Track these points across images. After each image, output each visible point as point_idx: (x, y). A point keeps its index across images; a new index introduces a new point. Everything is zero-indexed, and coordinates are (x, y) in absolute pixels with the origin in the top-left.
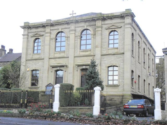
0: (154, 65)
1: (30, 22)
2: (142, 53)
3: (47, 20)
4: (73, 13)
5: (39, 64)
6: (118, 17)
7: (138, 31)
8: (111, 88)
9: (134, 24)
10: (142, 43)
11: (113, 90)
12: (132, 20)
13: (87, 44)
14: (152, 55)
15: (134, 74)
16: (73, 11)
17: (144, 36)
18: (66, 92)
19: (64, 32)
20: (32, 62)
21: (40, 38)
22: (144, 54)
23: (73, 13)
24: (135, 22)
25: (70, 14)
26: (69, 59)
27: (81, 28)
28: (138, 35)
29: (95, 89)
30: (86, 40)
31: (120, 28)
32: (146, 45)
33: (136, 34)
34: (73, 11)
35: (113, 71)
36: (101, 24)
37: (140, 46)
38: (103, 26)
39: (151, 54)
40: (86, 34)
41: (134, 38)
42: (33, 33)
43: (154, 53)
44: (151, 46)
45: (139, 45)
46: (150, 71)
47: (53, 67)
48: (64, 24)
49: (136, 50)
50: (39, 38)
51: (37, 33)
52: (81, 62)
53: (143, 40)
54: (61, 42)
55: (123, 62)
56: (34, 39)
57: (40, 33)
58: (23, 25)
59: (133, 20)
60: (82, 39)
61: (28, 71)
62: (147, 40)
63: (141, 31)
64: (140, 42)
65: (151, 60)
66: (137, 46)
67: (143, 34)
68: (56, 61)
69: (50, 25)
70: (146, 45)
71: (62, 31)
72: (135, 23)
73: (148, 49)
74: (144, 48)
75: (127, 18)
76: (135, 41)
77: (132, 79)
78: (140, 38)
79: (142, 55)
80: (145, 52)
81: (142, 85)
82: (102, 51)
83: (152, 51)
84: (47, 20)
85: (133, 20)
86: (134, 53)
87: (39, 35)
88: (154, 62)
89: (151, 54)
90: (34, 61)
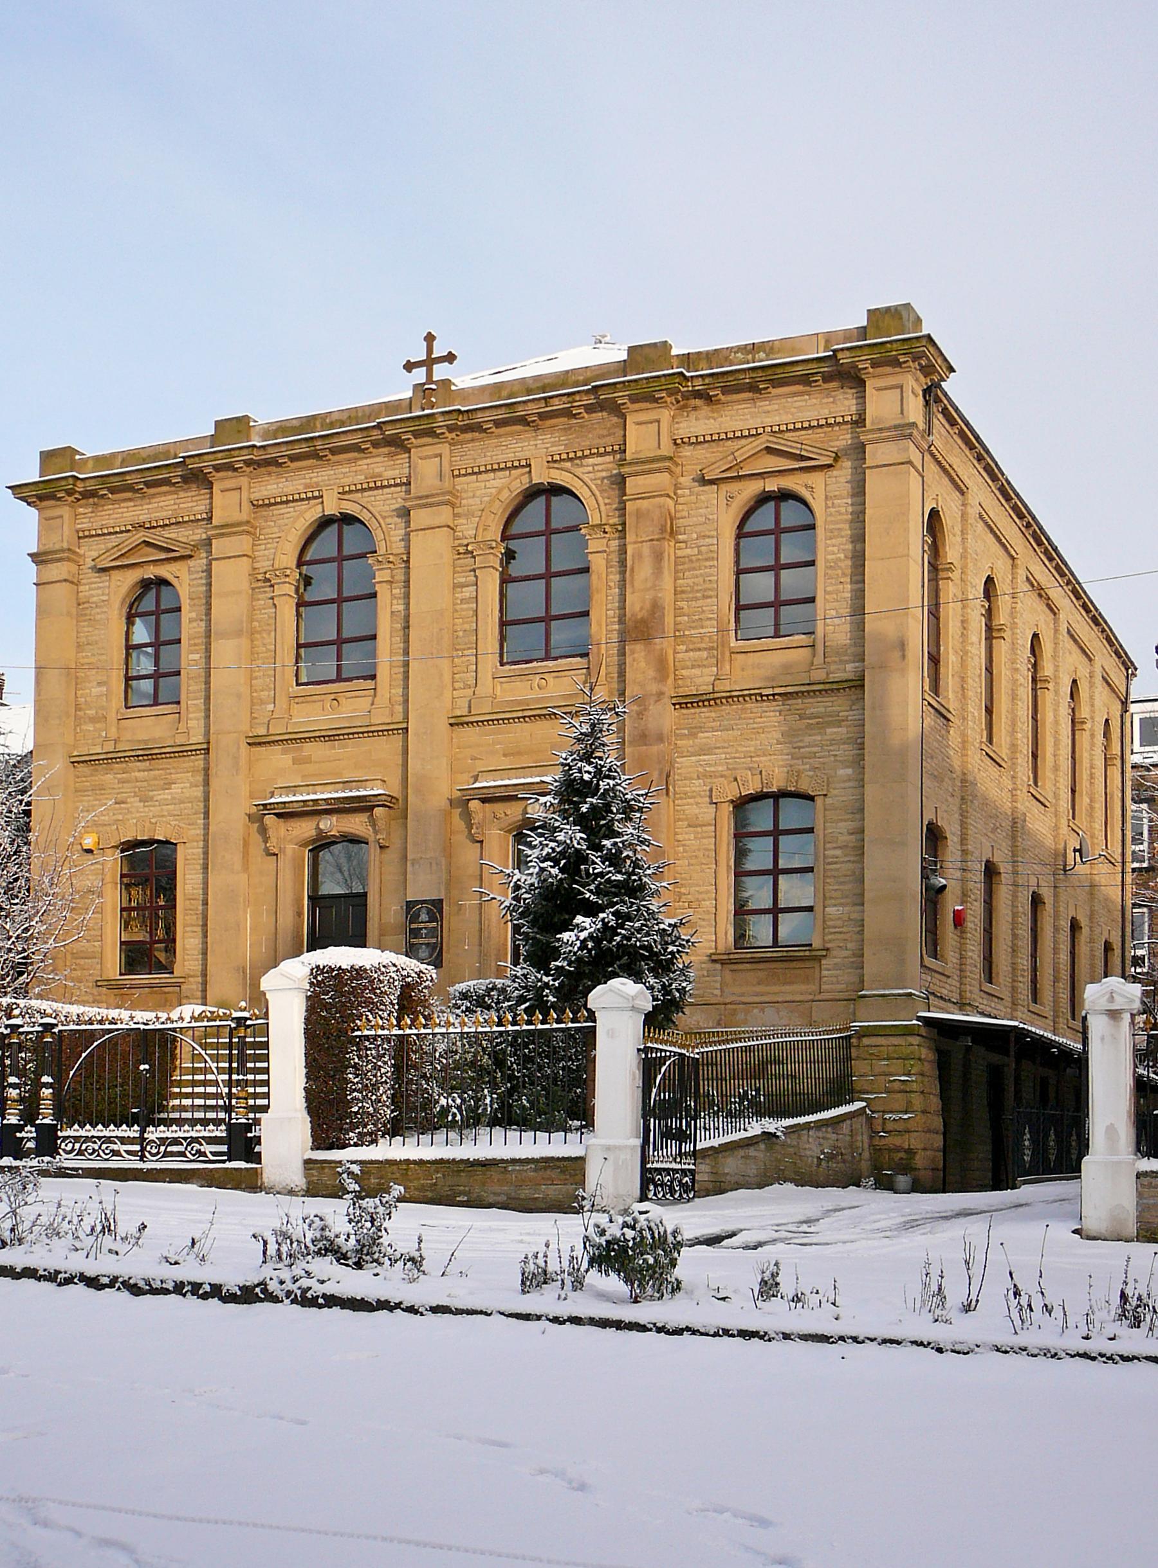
0: (1115, 772)
1: (90, 448)
2: (1015, 681)
3: (218, 424)
4: (430, 350)
5: (176, 789)
6: (805, 380)
7: (981, 492)
8: (761, 974)
9: (942, 437)
10: (1014, 596)
11: (776, 989)
12: (927, 403)
13: (554, 612)
14: (1101, 694)
15: (952, 851)
16: (430, 338)
17: (1038, 537)
18: (13, 1080)
19: (364, 516)
20: (121, 781)
21: (170, 578)
22: (1034, 680)
23: (430, 350)
24: (953, 416)
25: (409, 366)
26: (245, 727)
27: (496, 481)
28: (1067, 638)
29: (598, 997)
30: (548, 576)
31: (830, 466)
32: (1052, 609)
33: (964, 516)
34: (430, 338)
35: (770, 840)
36: (666, 441)
37: (1002, 618)
38: (687, 451)
39: (1092, 685)
40: (548, 532)
41: (951, 553)
42: (114, 540)
43: (1118, 679)
44: (1097, 620)
45: (989, 614)
46: (1082, 821)
47: (286, 814)
48: (356, 448)
49: (964, 655)
50: (162, 582)
51: (150, 537)
52: (506, 763)
53: (1022, 574)
54: (340, 600)
55: (859, 761)
56: (124, 589)
57: (172, 533)
58: (31, 474)
59: (933, 394)
60: (515, 569)
61: (89, 851)
62: (1061, 569)
63: (1006, 492)
64: (1083, 686)
65: (1092, 736)
66: (977, 623)
67: (1021, 512)
68: (308, 760)
69: (248, 463)
70: (1052, 609)
71: (350, 508)
72: (952, 423)
73: (1070, 644)
74: (989, 581)
75: (881, 383)
76: (956, 575)
77: (933, 896)
78: (1001, 552)
79: (1014, 697)
80: (1047, 669)
81: (1015, 936)
82: (684, 672)
83: (1104, 659)
84: (218, 424)
85: (938, 400)
86: (949, 681)
87: (163, 556)
88: (1116, 749)
89: (1092, 685)
90: (138, 771)
